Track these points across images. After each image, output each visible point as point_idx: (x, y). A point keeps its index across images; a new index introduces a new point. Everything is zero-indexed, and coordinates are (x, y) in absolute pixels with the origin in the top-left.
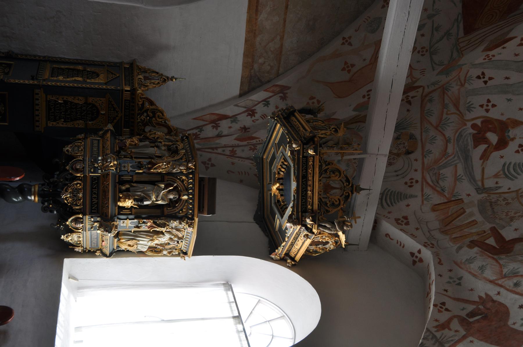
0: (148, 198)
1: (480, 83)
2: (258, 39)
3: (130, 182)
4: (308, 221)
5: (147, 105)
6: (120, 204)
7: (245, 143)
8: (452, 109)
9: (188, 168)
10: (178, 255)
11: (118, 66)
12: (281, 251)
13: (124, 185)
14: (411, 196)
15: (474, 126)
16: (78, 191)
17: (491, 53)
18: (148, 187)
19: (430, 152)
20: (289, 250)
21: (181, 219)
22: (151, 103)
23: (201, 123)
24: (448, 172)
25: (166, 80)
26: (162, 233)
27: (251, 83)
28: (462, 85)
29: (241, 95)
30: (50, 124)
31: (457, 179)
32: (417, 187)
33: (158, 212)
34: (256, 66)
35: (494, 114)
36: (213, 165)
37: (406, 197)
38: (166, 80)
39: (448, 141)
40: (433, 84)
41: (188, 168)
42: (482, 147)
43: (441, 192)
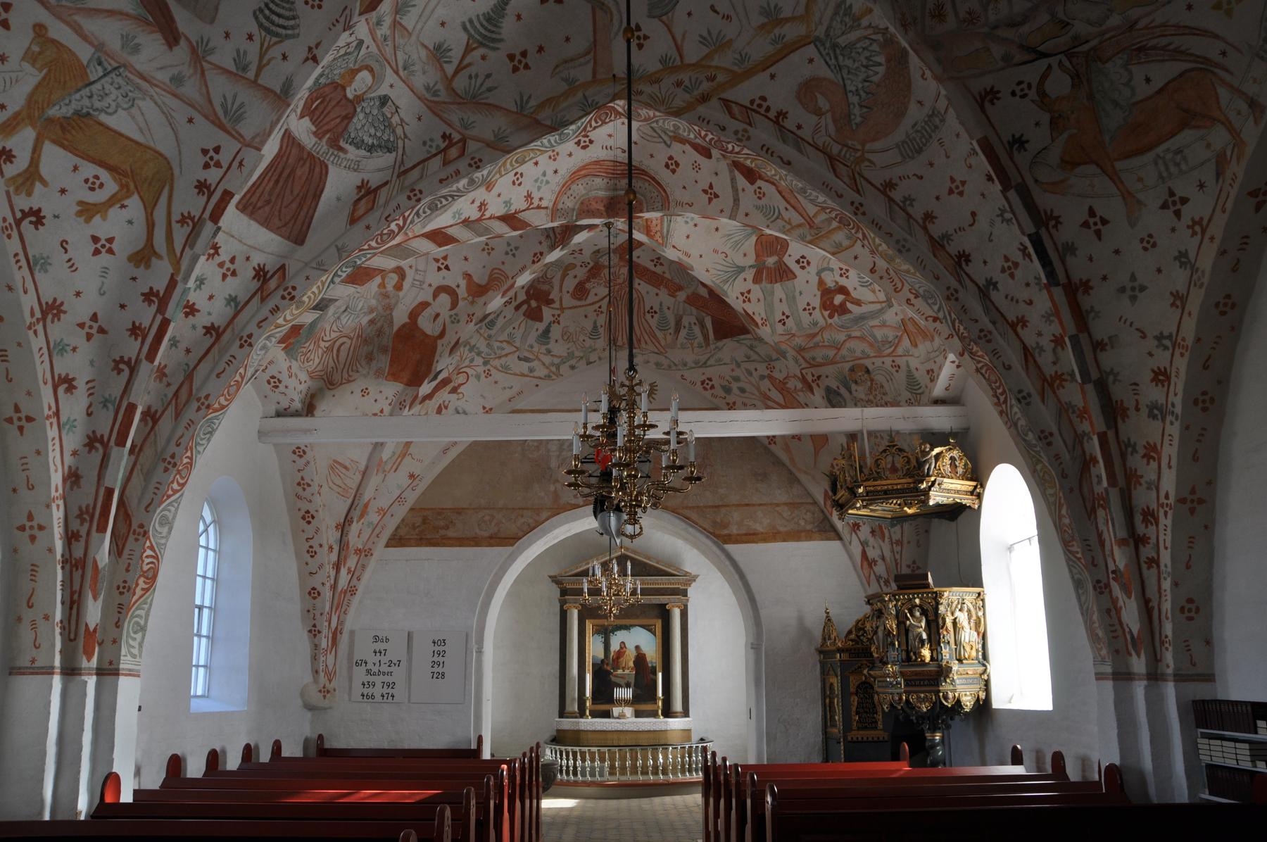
0: (920, 635)
1: (790, 322)
2: (782, 529)
3: (908, 652)
4: (924, 486)
5: (853, 636)
6: (928, 659)
7: (886, 532)
8: (818, 338)
9: (890, 600)
10: (983, 600)
11: (823, 664)
12: (967, 501)
13: (910, 656)
14: (908, 366)
15: (831, 316)
16: (919, 698)
17: (760, 322)
18: (910, 635)
19: (863, 352)
20: (966, 493)
21: (938, 604)
22: (850, 632)
23: (873, 577)
24: (879, 334)
25: (829, 619)
26: (955, 623)
27: (826, 530)
28: (794, 335)
29: (840, 539)
30: (880, 726)
31: (884, 325)
32: (899, 361)
33: (933, 625)
34: (809, 527)
35: (816, 302)
36: (914, 562)
37: (909, 371)
38: (829, 619)
39: (850, 337)
40: (796, 361)
41: (890, 600)
42: (849, 305)
43: (900, 339)
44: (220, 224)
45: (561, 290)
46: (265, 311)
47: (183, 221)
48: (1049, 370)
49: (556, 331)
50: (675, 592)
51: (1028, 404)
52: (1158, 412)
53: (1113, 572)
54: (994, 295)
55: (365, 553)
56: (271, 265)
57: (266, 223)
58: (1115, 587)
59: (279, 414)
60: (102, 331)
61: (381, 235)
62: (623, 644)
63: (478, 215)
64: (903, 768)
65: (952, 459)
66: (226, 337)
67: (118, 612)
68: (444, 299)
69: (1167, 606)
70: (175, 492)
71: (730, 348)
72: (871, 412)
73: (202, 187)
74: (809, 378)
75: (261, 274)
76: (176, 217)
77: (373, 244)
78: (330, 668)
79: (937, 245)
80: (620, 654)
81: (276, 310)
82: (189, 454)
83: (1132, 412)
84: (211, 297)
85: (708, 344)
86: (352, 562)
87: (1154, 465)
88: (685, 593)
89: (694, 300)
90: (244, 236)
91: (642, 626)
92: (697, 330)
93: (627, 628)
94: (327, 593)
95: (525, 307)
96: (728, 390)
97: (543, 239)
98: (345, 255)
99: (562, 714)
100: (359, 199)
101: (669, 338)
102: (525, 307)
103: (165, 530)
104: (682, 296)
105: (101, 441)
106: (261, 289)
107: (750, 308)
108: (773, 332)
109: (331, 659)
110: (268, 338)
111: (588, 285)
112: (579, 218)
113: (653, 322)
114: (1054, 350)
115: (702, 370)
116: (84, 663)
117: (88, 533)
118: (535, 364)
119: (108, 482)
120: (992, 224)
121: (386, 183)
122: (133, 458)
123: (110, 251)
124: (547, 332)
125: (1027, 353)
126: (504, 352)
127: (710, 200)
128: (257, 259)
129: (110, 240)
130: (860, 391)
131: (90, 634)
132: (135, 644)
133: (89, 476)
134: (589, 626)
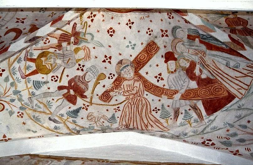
49: (83, 113)
95: (65, 91)
104: (177, 96)
111: (111, 94)
118: (61, 125)
124: (76, 112)
126: (39, 110)
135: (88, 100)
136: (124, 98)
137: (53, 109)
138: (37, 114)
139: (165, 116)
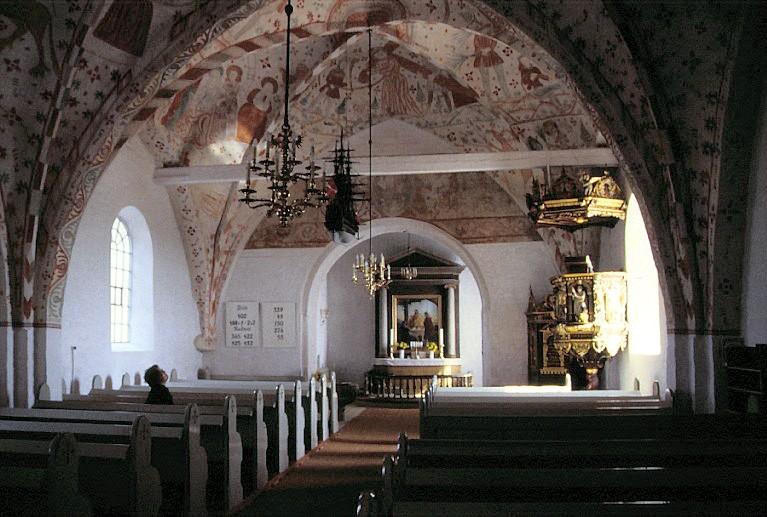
8: (521, 103)
12: (616, 214)
14: (581, 121)
15: (529, 88)
30: (562, 364)
32: (575, 118)
35: (519, 78)
42: (540, 80)
44: (83, 46)
45: (351, 76)
46: (120, 101)
47: (61, 46)
48: (640, 121)
49: (349, 105)
50: (450, 277)
51: (625, 145)
52: (709, 149)
53: (679, 261)
54: (602, 69)
55: (230, 253)
56: (123, 70)
57: (115, 44)
58: (679, 270)
59: (165, 166)
60: (18, 119)
61: (192, 46)
62: (416, 312)
63: (275, 29)
64: (565, 391)
65: (606, 185)
66: (98, 118)
67: (42, 289)
68: (269, 86)
69: (711, 285)
70: (74, 217)
71: (465, 112)
72: (556, 153)
73: (70, 23)
74: (516, 131)
75: (116, 76)
76: (56, 44)
77: (187, 52)
78: (212, 325)
79: (563, 35)
80: (414, 318)
81: (127, 99)
82: (80, 192)
83: (693, 151)
84: (85, 94)
85: (451, 110)
86: (223, 258)
87: (706, 186)
88: (457, 277)
89: (440, 80)
90: (102, 54)
91: (430, 300)
92: (443, 99)
93: (419, 300)
94: (207, 279)
95: (326, 90)
96: (464, 140)
97: (329, 43)
98: (169, 60)
99: (377, 356)
100: (176, 25)
101: (425, 107)
102: (326, 90)
103: (70, 240)
104: (432, 77)
105: (25, 186)
106: (117, 86)
107: (472, 85)
108: (490, 100)
109: (212, 319)
110: (124, 117)
112: (347, 27)
113: (414, 96)
114: (642, 107)
115: (449, 127)
116: (25, 321)
117: (23, 242)
119: (31, 212)
120: (597, 18)
121: (192, 12)
122: (45, 197)
123: (18, 68)
124: (343, 104)
125: (625, 108)
127: (431, 11)
128: (112, 68)
129: (17, 61)
130: (551, 140)
131: (28, 304)
132: (57, 309)
133: (21, 206)
134: (395, 300)
135: (349, 87)
136: (381, 76)
137: (324, 113)
138: (314, 126)
139: (420, 98)
